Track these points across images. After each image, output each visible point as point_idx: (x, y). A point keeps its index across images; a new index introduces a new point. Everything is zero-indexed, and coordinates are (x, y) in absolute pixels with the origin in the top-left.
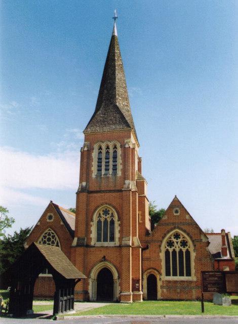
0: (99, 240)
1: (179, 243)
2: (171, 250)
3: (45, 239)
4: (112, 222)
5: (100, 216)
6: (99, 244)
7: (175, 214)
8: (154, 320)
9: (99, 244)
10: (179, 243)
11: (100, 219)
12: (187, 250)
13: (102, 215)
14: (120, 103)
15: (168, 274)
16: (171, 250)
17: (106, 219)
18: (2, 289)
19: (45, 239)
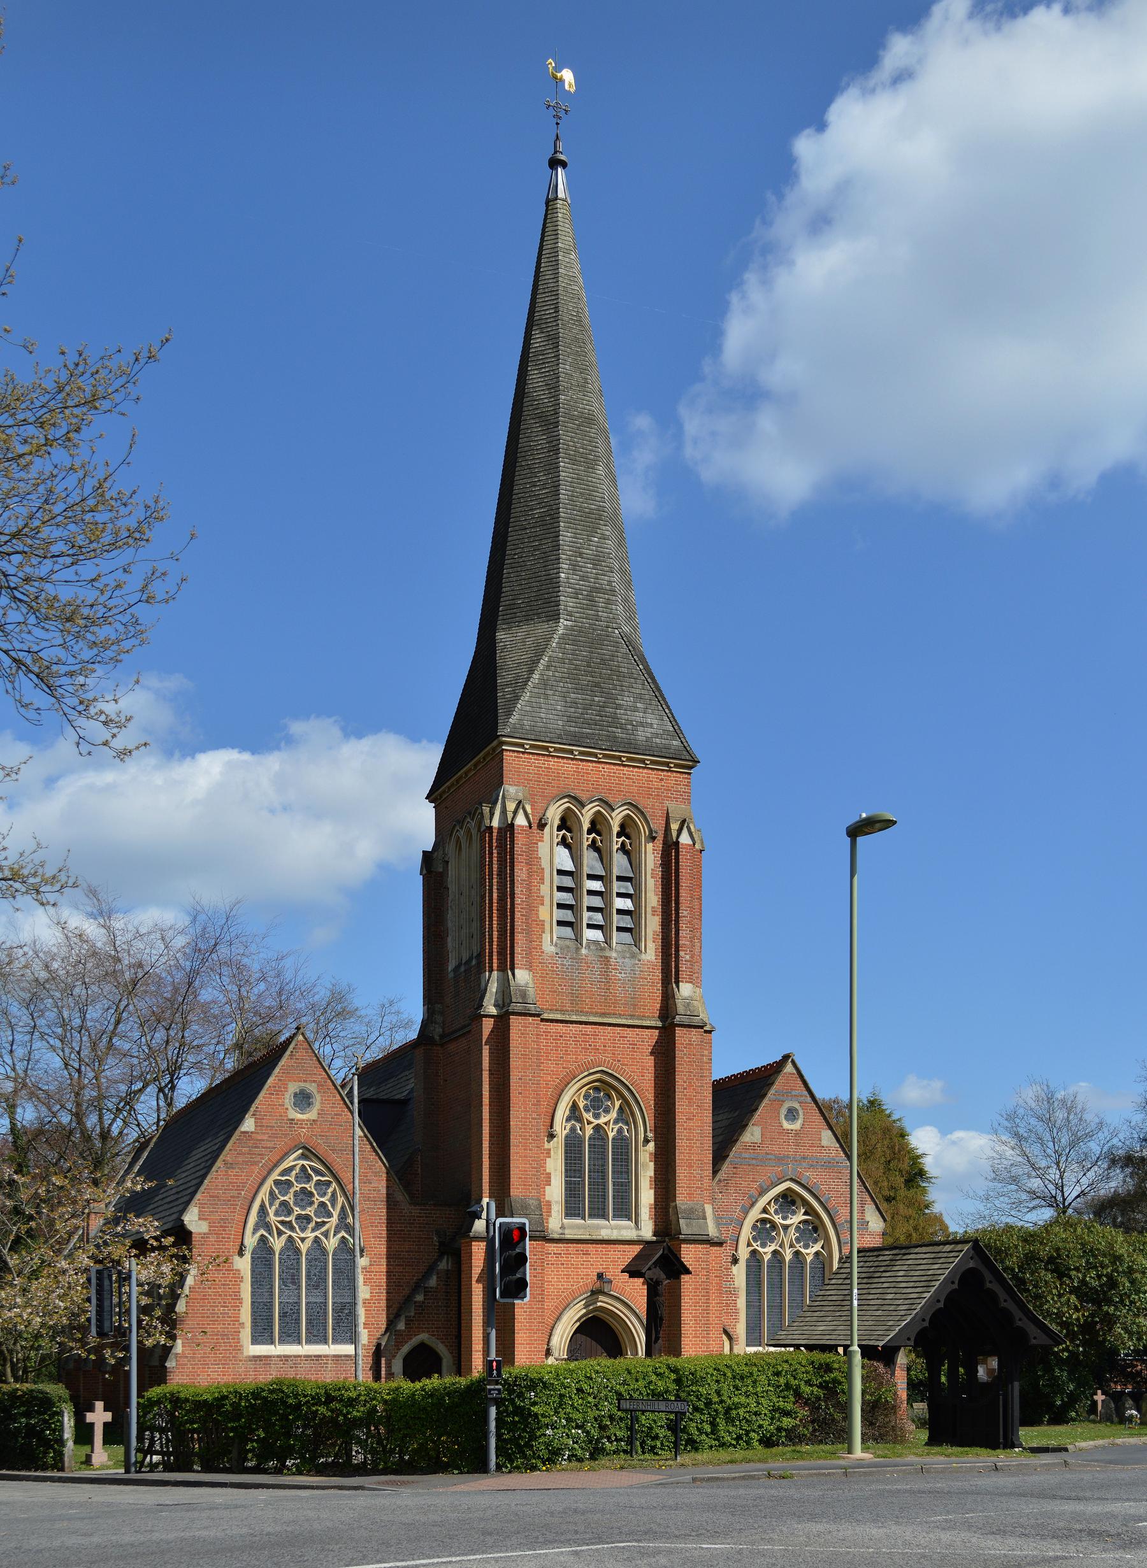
0: (572, 1209)
1: (792, 1230)
2: (767, 1252)
3: (289, 1212)
4: (623, 1148)
5: (574, 1113)
6: (577, 1227)
7: (786, 1125)
8: (778, 1490)
9: (577, 1227)
10: (792, 1230)
11: (573, 1129)
12: (775, 1252)
13: (587, 1116)
14: (997, 486)
15: (262, 1333)
16: (767, 1252)
17: (597, 1128)
18: (1145, 1527)
19: (322, 1204)
